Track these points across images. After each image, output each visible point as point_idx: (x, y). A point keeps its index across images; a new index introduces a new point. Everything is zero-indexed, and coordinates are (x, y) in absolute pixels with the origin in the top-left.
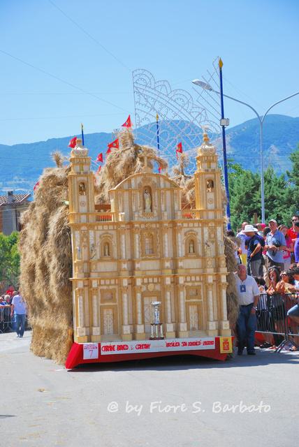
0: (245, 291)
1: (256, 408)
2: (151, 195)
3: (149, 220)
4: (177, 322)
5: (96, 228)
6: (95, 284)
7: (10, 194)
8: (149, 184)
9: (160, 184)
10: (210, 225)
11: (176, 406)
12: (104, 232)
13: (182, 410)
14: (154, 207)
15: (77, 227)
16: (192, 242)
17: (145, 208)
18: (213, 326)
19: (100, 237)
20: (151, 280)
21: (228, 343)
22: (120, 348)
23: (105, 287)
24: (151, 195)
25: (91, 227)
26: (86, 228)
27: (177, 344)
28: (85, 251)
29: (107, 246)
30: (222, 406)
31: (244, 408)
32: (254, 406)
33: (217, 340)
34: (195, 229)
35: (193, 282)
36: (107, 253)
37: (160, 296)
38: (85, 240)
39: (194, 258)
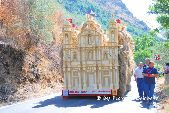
3: (90, 46)
22: (76, 92)
34: (107, 50)
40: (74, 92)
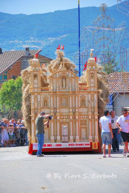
0: (113, 123)
1: (110, 176)
2: (66, 80)
4: (75, 135)
5: (41, 94)
6: (77, 117)
7: (27, 49)
8: (65, 75)
9: (69, 75)
10: (92, 93)
11: (76, 175)
12: (45, 96)
13: (78, 177)
14: (67, 85)
15: (33, 93)
16: (83, 101)
17: (63, 85)
18: (90, 137)
19: (43, 98)
20: (65, 117)
21: (96, 145)
22: (49, 145)
23: (82, 119)
24: (66, 80)
25: (39, 93)
26: (37, 94)
27: (73, 145)
28: (36, 104)
29: (46, 102)
30: (96, 175)
31: (105, 176)
32: (110, 175)
33: (91, 143)
35: (83, 118)
36: (46, 105)
37: (68, 123)
38: (36, 99)
39: (84, 108)
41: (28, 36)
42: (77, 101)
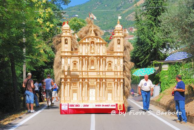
0: (146, 85)
22: (77, 106)
27: (100, 106)
33: (117, 104)
40: (75, 106)
41: (112, 15)
42: (110, 80)
